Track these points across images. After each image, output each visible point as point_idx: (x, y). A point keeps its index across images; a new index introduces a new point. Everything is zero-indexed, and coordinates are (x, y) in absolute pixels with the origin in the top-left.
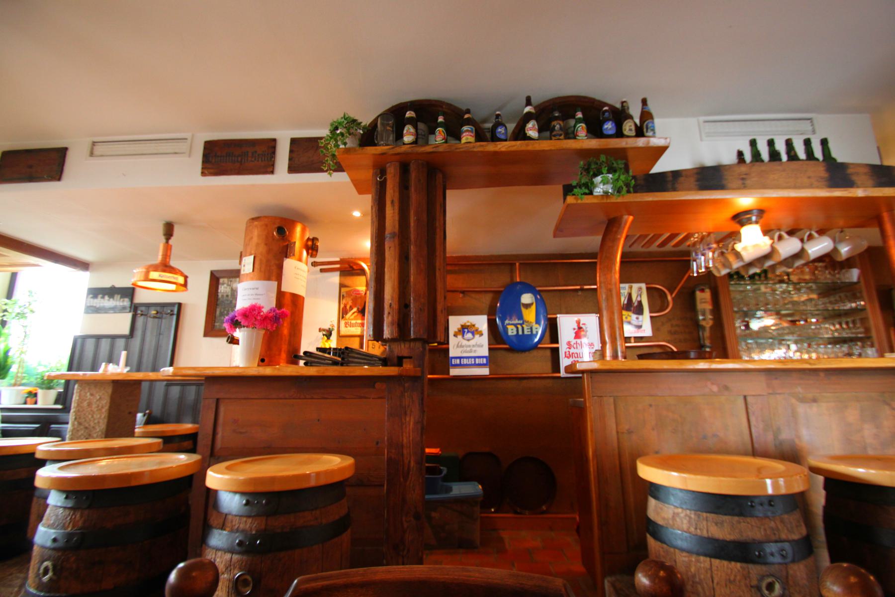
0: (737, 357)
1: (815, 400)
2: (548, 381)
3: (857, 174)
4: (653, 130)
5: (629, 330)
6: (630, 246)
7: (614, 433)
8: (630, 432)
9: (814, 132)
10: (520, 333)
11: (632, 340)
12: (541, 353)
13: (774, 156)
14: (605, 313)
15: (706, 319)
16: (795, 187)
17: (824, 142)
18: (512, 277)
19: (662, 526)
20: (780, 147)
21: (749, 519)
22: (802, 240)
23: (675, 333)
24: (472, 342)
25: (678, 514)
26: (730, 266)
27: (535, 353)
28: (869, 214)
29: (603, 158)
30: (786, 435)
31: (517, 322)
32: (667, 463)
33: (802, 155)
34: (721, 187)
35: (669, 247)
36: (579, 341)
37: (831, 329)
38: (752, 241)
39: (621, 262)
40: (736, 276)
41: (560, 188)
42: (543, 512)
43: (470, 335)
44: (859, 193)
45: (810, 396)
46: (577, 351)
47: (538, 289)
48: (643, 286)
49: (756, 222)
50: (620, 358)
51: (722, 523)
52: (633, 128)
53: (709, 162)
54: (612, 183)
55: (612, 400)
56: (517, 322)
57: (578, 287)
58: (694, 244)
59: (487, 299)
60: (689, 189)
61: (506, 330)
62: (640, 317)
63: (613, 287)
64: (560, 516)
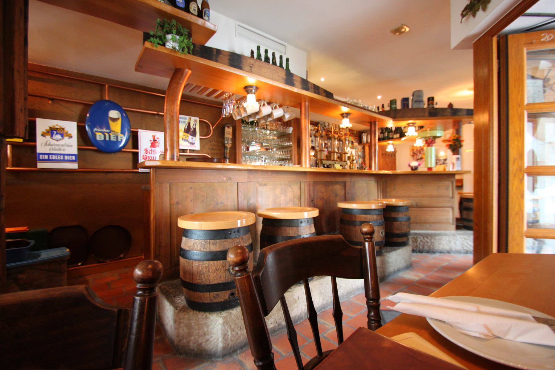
0: (240, 163)
1: (265, 185)
2: (129, 174)
3: (296, 80)
4: (208, 17)
5: (183, 145)
6: (190, 91)
7: (168, 204)
8: (178, 203)
9: (285, 53)
10: (107, 139)
11: (188, 151)
12: (125, 155)
13: (267, 59)
14: (168, 131)
15: (228, 144)
16: (272, 79)
17: (287, 60)
18: (102, 96)
19: (187, 251)
20: (270, 56)
21: (228, 240)
22: (272, 108)
23: (213, 149)
24: (60, 143)
25: (196, 243)
26: (241, 116)
27: (119, 155)
28: (297, 101)
29: (174, 22)
30: (252, 201)
31: (104, 130)
32: (194, 217)
33: (278, 64)
34: (240, 67)
35: (212, 98)
36: (153, 149)
37: (279, 154)
38: (251, 104)
39: (181, 101)
40: (243, 121)
41: (141, 34)
42: (121, 258)
43: (59, 137)
44: (295, 90)
45: (264, 183)
46: (152, 156)
47: (124, 108)
48: (198, 119)
49: (254, 94)
50: (175, 160)
51: (216, 244)
52: (196, 9)
53: (238, 51)
54: (179, 43)
55: (168, 185)
56: (104, 130)
57: (155, 113)
58: (225, 99)
59: (77, 109)
60: (224, 64)
61: (94, 136)
62: (194, 138)
63: (175, 114)
64: (134, 258)
